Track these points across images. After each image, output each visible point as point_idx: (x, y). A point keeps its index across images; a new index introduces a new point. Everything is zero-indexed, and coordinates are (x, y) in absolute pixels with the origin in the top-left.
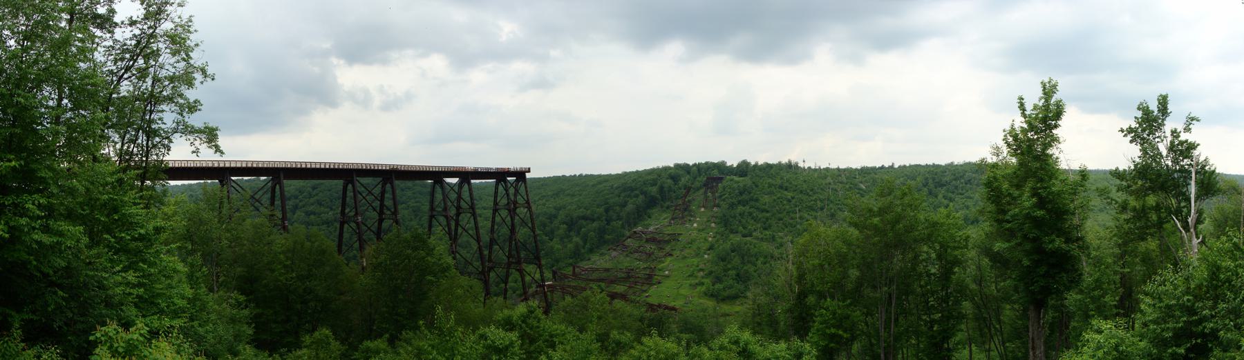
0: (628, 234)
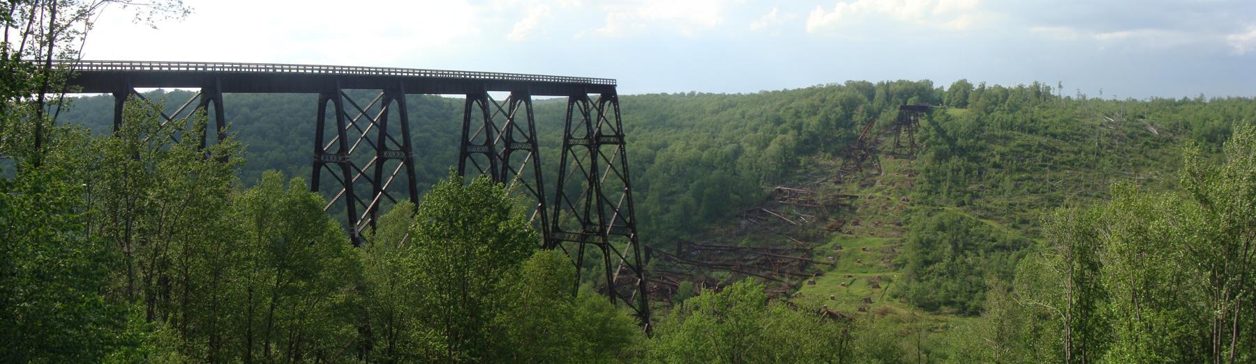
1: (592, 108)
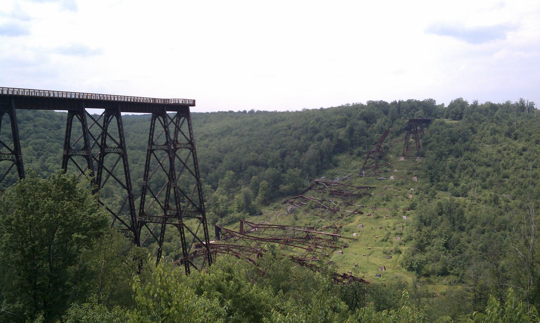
1: (170, 122)
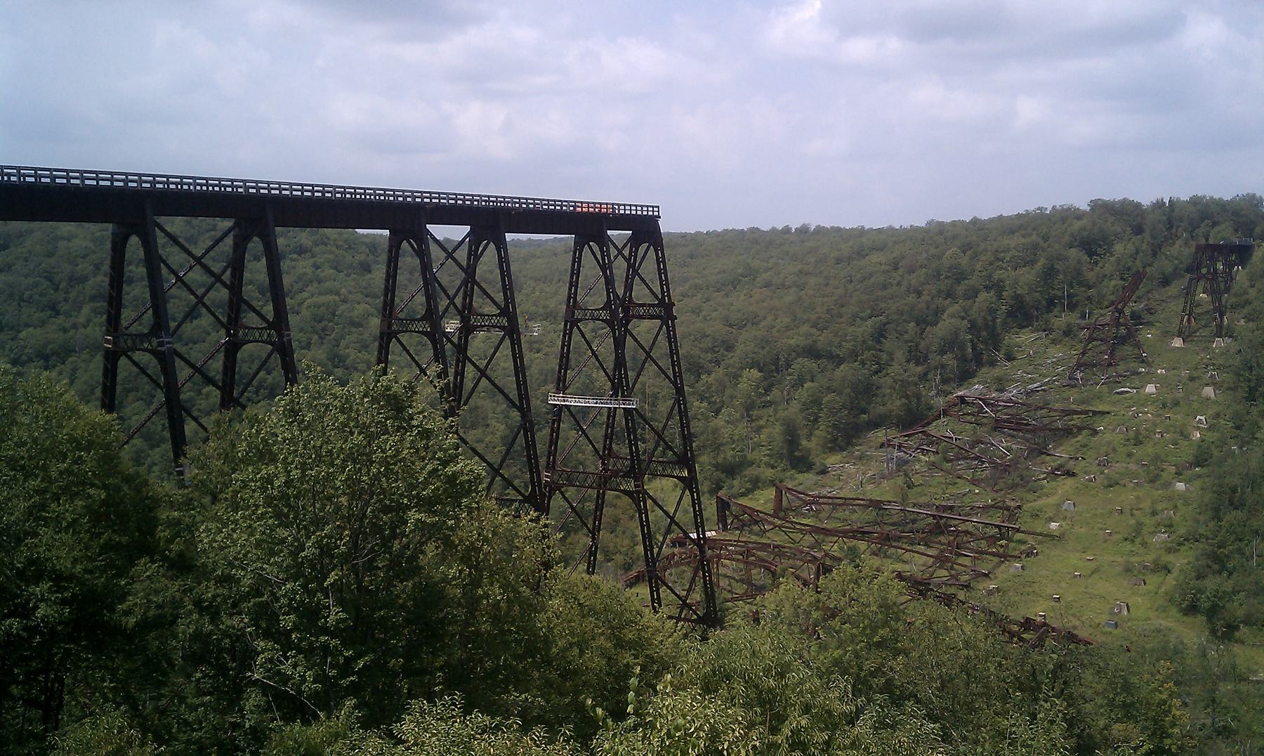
0: (940, 402)
1: (616, 257)
